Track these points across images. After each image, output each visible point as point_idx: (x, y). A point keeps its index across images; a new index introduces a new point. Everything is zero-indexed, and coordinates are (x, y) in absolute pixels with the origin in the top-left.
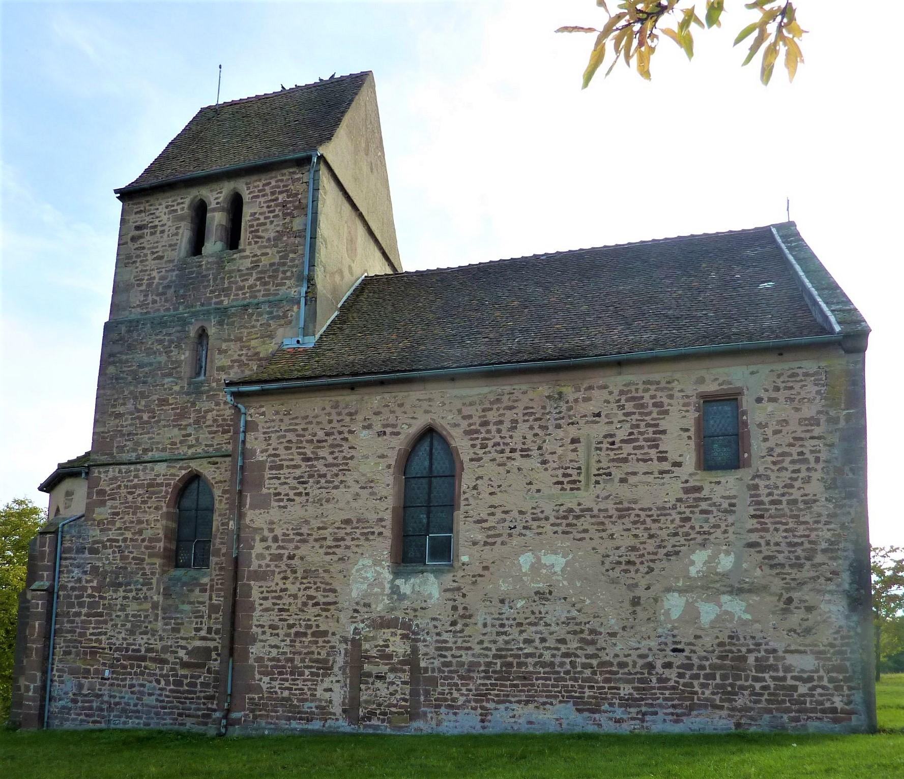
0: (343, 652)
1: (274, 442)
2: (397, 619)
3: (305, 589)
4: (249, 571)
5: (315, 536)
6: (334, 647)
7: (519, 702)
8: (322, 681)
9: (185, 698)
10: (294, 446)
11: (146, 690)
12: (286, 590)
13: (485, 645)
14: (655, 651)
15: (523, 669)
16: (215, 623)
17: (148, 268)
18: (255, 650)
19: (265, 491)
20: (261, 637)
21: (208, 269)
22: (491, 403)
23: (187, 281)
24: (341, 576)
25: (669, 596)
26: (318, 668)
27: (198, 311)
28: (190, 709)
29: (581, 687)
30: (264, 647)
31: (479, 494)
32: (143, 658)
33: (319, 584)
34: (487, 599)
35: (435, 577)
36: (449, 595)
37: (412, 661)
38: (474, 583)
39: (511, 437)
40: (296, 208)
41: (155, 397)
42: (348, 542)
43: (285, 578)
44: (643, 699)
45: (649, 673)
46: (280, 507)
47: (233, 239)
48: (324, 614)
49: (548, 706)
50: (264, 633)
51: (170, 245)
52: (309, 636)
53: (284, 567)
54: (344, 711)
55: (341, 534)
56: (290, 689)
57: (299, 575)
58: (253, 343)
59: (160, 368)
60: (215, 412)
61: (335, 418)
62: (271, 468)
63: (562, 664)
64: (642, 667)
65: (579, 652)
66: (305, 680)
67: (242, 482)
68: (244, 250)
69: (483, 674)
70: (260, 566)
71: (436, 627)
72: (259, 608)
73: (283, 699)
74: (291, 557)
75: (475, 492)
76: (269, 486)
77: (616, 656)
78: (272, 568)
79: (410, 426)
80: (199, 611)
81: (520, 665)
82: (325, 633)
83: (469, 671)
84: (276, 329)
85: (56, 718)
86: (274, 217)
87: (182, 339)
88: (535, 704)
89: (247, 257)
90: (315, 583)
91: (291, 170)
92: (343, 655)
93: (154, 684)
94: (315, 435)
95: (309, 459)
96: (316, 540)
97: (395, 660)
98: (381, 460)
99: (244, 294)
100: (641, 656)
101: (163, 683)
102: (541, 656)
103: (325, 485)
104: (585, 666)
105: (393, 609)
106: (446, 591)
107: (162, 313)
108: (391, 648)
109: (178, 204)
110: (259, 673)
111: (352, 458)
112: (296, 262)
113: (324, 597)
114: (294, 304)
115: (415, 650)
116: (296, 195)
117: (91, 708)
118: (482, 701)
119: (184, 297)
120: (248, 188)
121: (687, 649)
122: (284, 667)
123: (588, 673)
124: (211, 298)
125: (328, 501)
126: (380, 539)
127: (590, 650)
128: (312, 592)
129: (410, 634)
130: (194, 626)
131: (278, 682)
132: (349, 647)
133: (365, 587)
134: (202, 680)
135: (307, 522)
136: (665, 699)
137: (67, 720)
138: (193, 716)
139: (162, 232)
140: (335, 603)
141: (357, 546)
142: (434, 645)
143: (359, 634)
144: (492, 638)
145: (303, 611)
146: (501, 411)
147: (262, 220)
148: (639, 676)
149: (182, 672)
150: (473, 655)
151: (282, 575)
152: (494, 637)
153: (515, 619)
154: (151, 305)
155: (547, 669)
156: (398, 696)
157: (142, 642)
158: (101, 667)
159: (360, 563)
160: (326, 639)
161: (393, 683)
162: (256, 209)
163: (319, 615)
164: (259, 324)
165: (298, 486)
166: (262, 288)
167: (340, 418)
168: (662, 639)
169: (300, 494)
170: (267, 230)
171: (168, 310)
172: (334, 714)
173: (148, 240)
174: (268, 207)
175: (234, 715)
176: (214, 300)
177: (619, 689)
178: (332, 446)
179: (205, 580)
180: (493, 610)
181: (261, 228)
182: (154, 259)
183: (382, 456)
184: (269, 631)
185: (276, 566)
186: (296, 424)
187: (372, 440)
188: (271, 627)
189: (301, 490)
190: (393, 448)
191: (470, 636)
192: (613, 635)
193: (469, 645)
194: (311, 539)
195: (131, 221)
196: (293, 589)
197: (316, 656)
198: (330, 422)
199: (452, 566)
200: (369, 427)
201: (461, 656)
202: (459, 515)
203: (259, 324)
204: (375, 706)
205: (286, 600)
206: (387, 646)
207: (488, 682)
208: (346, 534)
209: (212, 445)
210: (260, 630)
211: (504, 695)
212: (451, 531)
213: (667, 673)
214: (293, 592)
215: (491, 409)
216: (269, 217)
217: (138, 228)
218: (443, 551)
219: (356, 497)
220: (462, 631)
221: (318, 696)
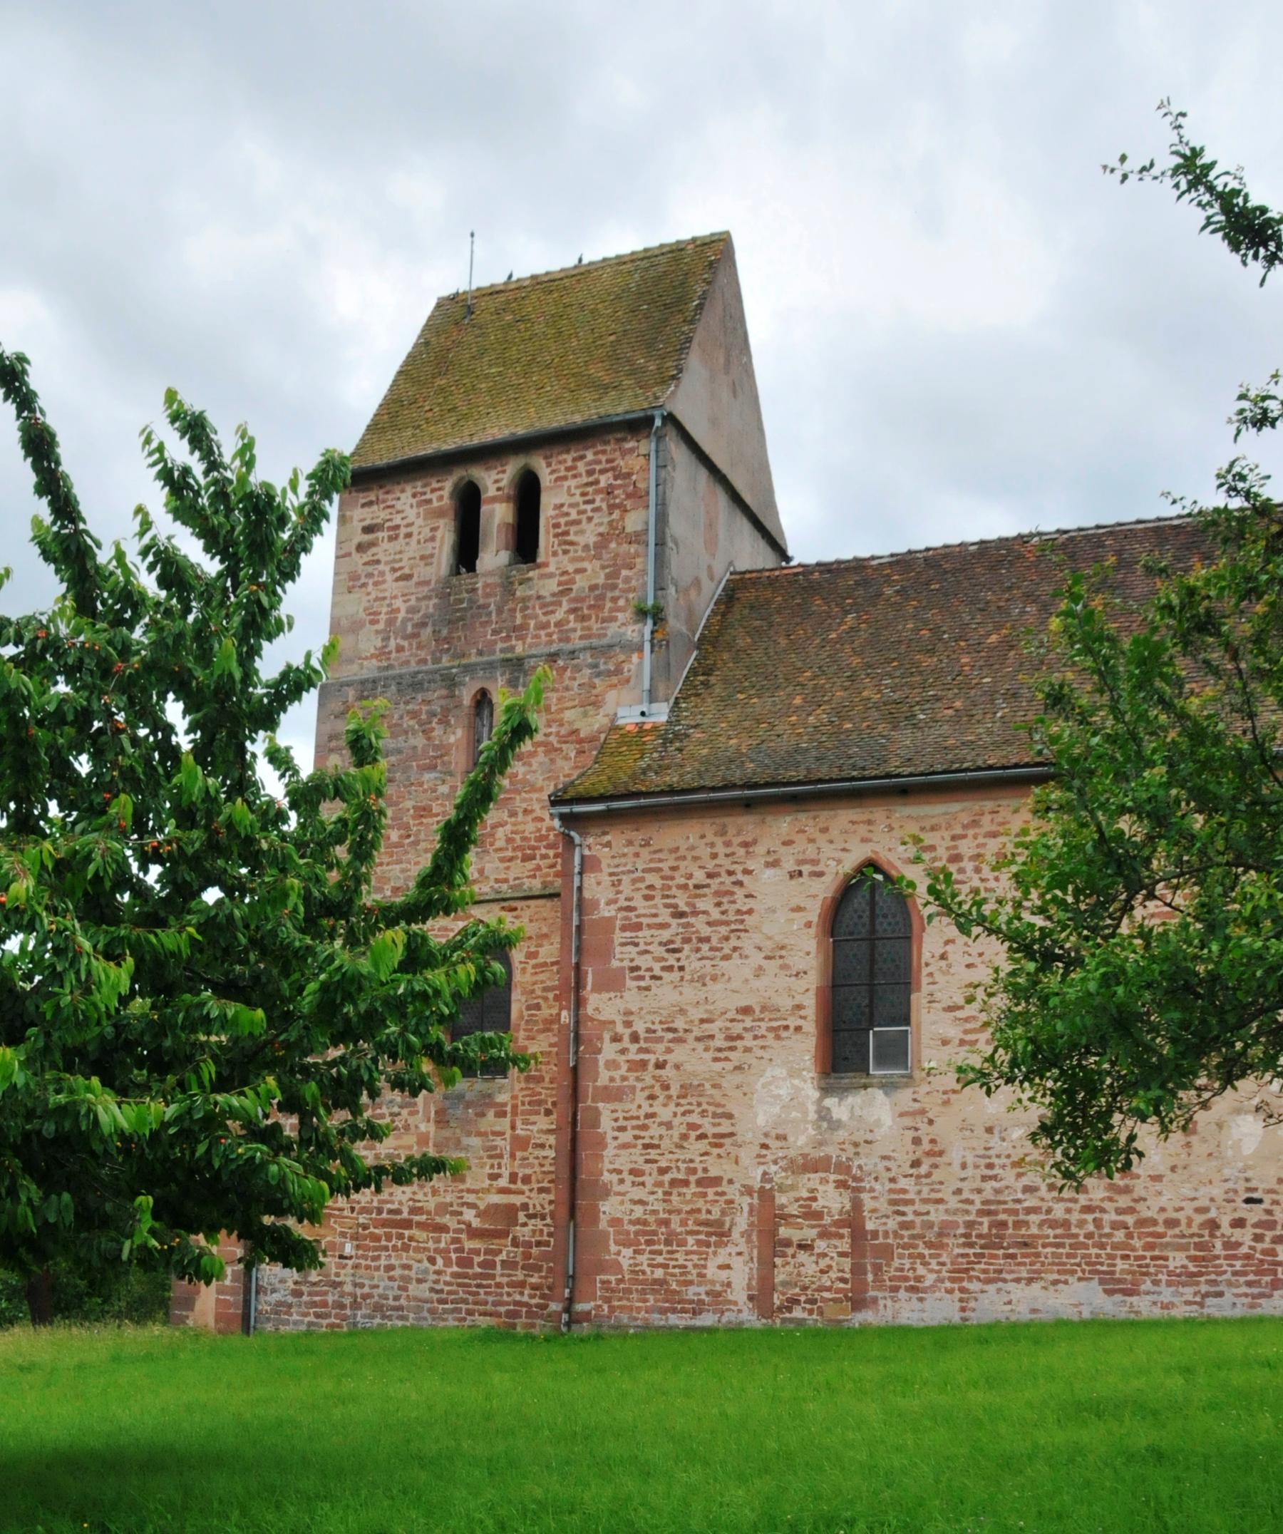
0: (746, 1209)
1: (626, 887)
2: (828, 1158)
3: (684, 1114)
4: (595, 1088)
5: (697, 1032)
6: (732, 1202)
7: (1018, 1280)
8: (715, 1253)
9: (478, 1286)
10: (657, 894)
11: (413, 1274)
12: (653, 1115)
13: (966, 1195)
14: (1219, 1201)
15: (1023, 1231)
16: (521, 1166)
17: (387, 594)
18: (609, 1208)
19: (615, 964)
20: (617, 1188)
21: (487, 595)
22: (965, 827)
23: (453, 614)
24: (739, 1093)
25: (1240, 1119)
26: (709, 1234)
27: (476, 664)
28: (486, 1303)
29: (1110, 1257)
30: (622, 1203)
31: (950, 966)
32: (407, 1224)
33: (705, 1106)
34: (966, 1127)
35: (886, 1094)
36: (908, 1121)
37: (853, 1222)
38: (946, 1103)
39: (997, 879)
40: (629, 496)
41: (409, 804)
42: (748, 1042)
43: (652, 1097)
44: (1201, 1274)
45: (1212, 1235)
46: (639, 988)
47: (525, 544)
48: (715, 1151)
49: (1061, 1286)
50: (622, 1181)
51: (422, 558)
52: (693, 1185)
53: (649, 1081)
54: (751, 1298)
55: (737, 1029)
56: (665, 1266)
57: (674, 1091)
58: (568, 715)
59: (414, 757)
60: (508, 827)
61: (721, 850)
62: (624, 929)
63: (1081, 1223)
64: (1202, 1226)
65: (1107, 1205)
66: (687, 1253)
67: (579, 950)
68: (546, 565)
69: (962, 1240)
70: (612, 1079)
71: (888, 1169)
72: (612, 1144)
73: (655, 1281)
74: (660, 1065)
75: (943, 963)
76: (622, 957)
77: (1163, 1210)
78: (631, 1082)
79: (839, 862)
80: (495, 1148)
81: (1018, 1224)
82: (717, 1181)
83: (940, 1235)
84: (605, 692)
85: (268, 1320)
86: (594, 510)
87: (449, 710)
88: (1042, 1283)
89: (551, 575)
90: (699, 1104)
91: (619, 436)
92: (746, 1214)
93: (426, 1264)
94: (690, 876)
95: (682, 915)
96: (698, 1039)
97: (827, 1220)
98: (795, 915)
99: (549, 635)
100: (1199, 1210)
101: (440, 1261)
102: (1049, 1211)
103: (709, 954)
104: (1115, 1226)
105: (821, 1144)
106: (901, 1115)
107: (413, 667)
108: (821, 1202)
109: (433, 491)
110: (616, 1243)
111: (750, 912)
112: (634, 583)
113: (714, 1125)
114: (633, 651)
115: (857, 1205)
116: (629, 475)
117: (325, 1304)
118: (962, 1280)
119: (447, 640)
120: (549, 465)
121: (1267, 1199)
122: (654, 1233)
123: (1120, 1235)
124: (495, 642)
125: (714, 978)
126: (799, 1036)
127: (1123, 1201)
128: (694, 1118)
129: (849, 1182)
130: (487, 1170)
131: (647, 1256)
132: (756, 1201)
133: (777, 1110)
134: (503, 1256)
135: (682, 1011)
136: (1235, 1273)
137: (287, 1322)
138: (491, 1315)
139: (409, 535)
140: (732, 1134)
141: (763, 1047)
142: (887, 1197)
143: (771, 1181)
144: (975, 1186)
145: (682, 1147)
146: (981, 840)
147: (574, 516)
148: (1196, 1239)
149: (469, 1245)
150: (947, 1211)
151: (647, 1093)
152: (978, 1184)
153: (1008, 1156)
154: (394, 655)
155: (1059, 1231)
156: (833, 1275)
157: (404, 1198)
158: (338, 1240)
159: (768, 1074)
160: (719, 1189)
161: (825, 1255)
162: (563, 498)
163: (706, 1154)
164: (576, 684)
165: (666, 955)
166: (579, 626)
167: (728, 851)
168: (1230, 1185)
169: (670, 969)
170: (582, 532)
171: (424, 661)
172: (735, 1303)
173: (384, 549)
174: (583, 494)
175: (580, 1307)
176: (500, 645)
177: (1166, 1259)
178: (717, 893)
179: (502, 1098)
180: (975, 1143)
181: (573, 529)
182: (397, 580)
183: (799, 909)
184: (629, 1179)
185: (638, 1079)
186: (660, 860)
187: (784, 882)
188: (632, 1172)
189: (672, 962)
190: (815, 896)
191: (941, 1183)
192: (1157, 1178)
193: (939, 1196)
194: (690, 1037)
195: (356, 518)
196: (665, 1113)
197: (704, 1216)
198: (714, 856)
199: (910, 1077)
200: (775, 864)
201: (928, 1213)
202: (918, 1000)
203: (576, 684)
204: (797, 1290)
205: (655, 1131)
206: (815, 1199)
207: (971, 1251)
208: (745, 1029)
209: (506, 881)
210: (615, 1177)
211: (995, 1271)
212: (907, 1021)
213: (1238, 1235)
214: (665, 1119)
215: (964, 837)
216: (584, 512)
217: (368, 529)
218: (896, 1053)
219: (759, 972)
220: (928, 1175)
221: (709, 1276)
